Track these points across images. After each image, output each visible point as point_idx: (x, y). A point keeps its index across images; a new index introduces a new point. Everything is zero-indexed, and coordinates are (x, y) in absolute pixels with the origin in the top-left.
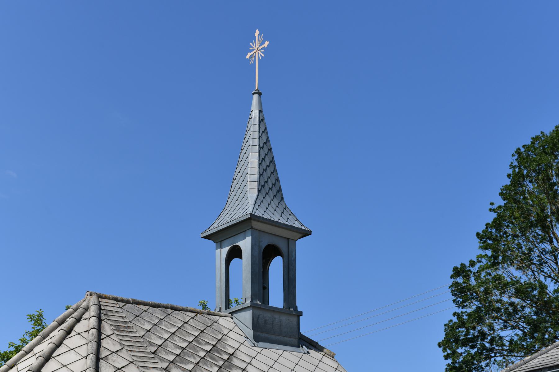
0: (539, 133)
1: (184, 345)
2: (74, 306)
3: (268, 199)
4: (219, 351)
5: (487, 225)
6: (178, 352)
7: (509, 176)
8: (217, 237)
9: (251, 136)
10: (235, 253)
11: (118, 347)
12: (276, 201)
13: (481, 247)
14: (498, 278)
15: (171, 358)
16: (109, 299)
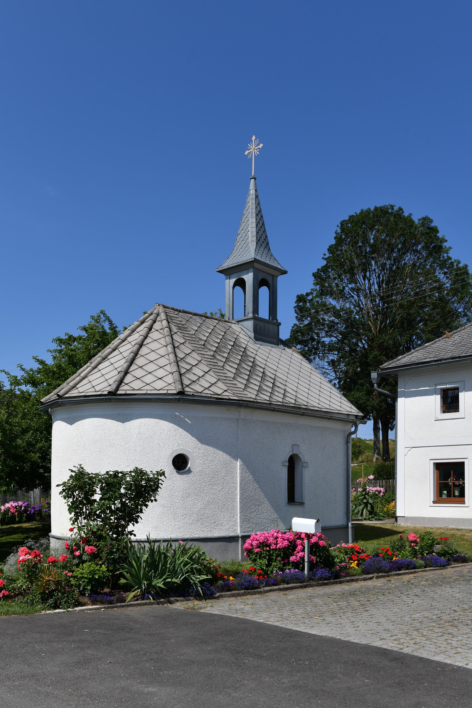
2: (149, 312)
3: (262, 249)
4: (239, 346)
5: (318, 270)
8: (227, 272)
9: (251, 206)
11: (183, 341)
12: (266, 251)
13: (314, 284)
14: (324, 305)
16: (169, 308)
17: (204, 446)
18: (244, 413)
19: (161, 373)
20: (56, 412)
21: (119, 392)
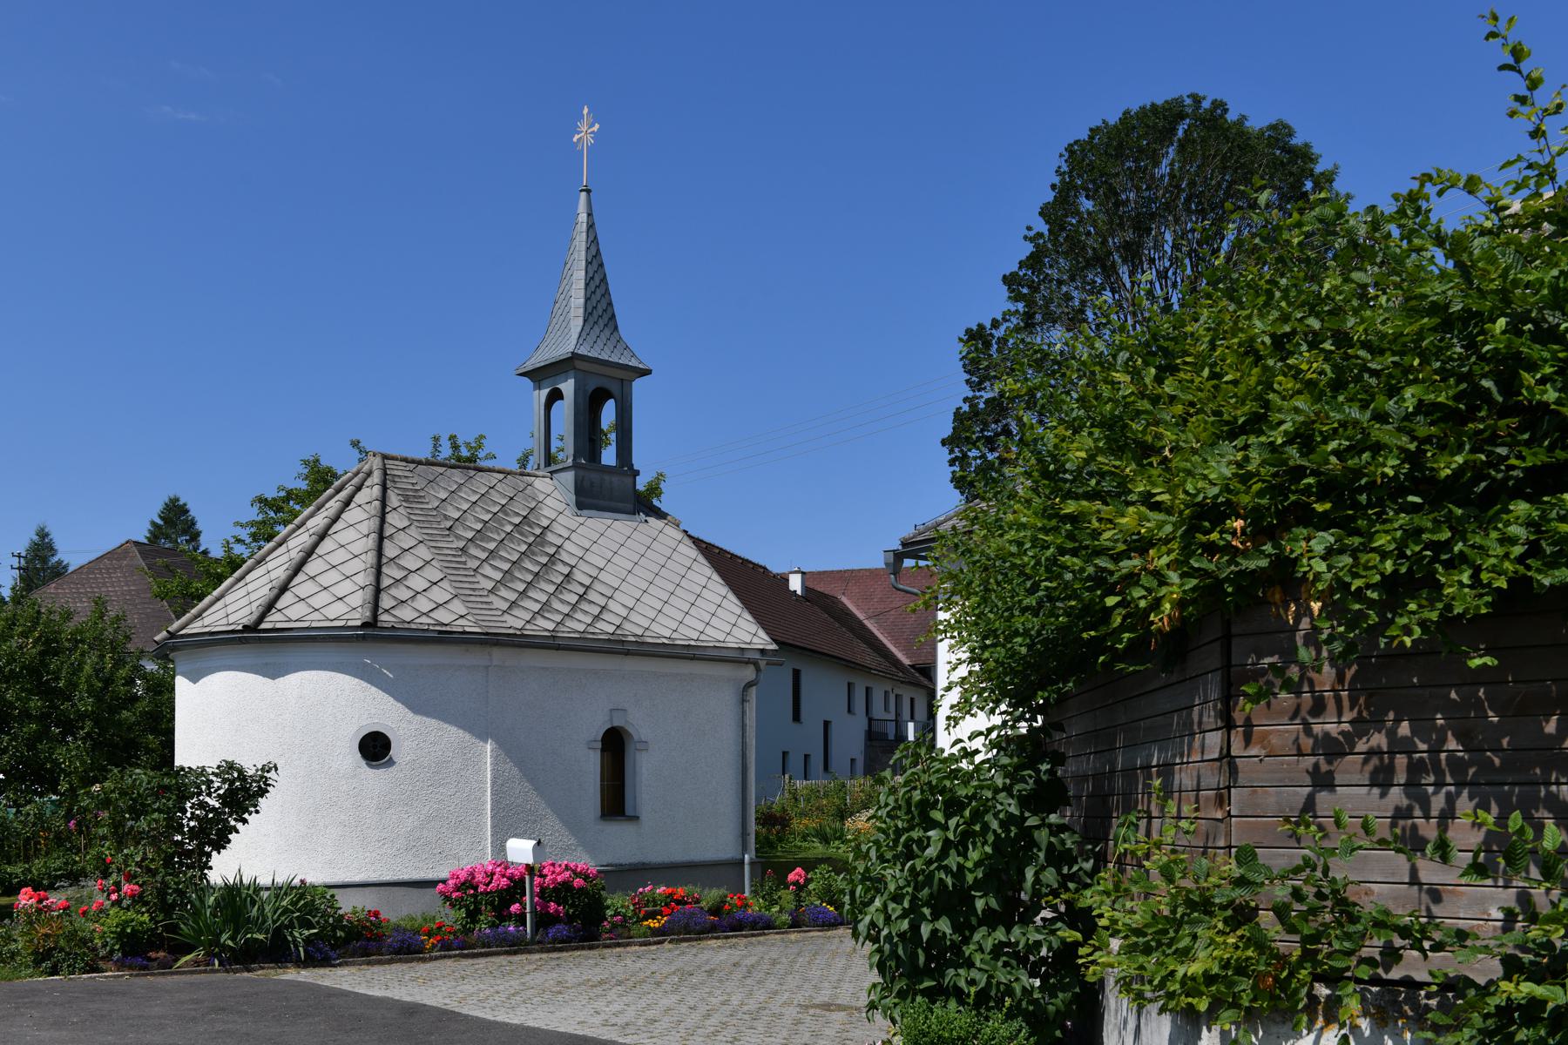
0: (1099, 123)
1: (487, 517)
3: (597, 329)
6: (479, 526)
7: (1053, 187)
8: (537, 375)
10: (555, 396)
11: (406, 523)
12: (607, 332)
15: (470, 535)
17: (418, 718)
18: (498, 655)
19: (345, 588)
20: (181, 660)
21: (263, 626)
